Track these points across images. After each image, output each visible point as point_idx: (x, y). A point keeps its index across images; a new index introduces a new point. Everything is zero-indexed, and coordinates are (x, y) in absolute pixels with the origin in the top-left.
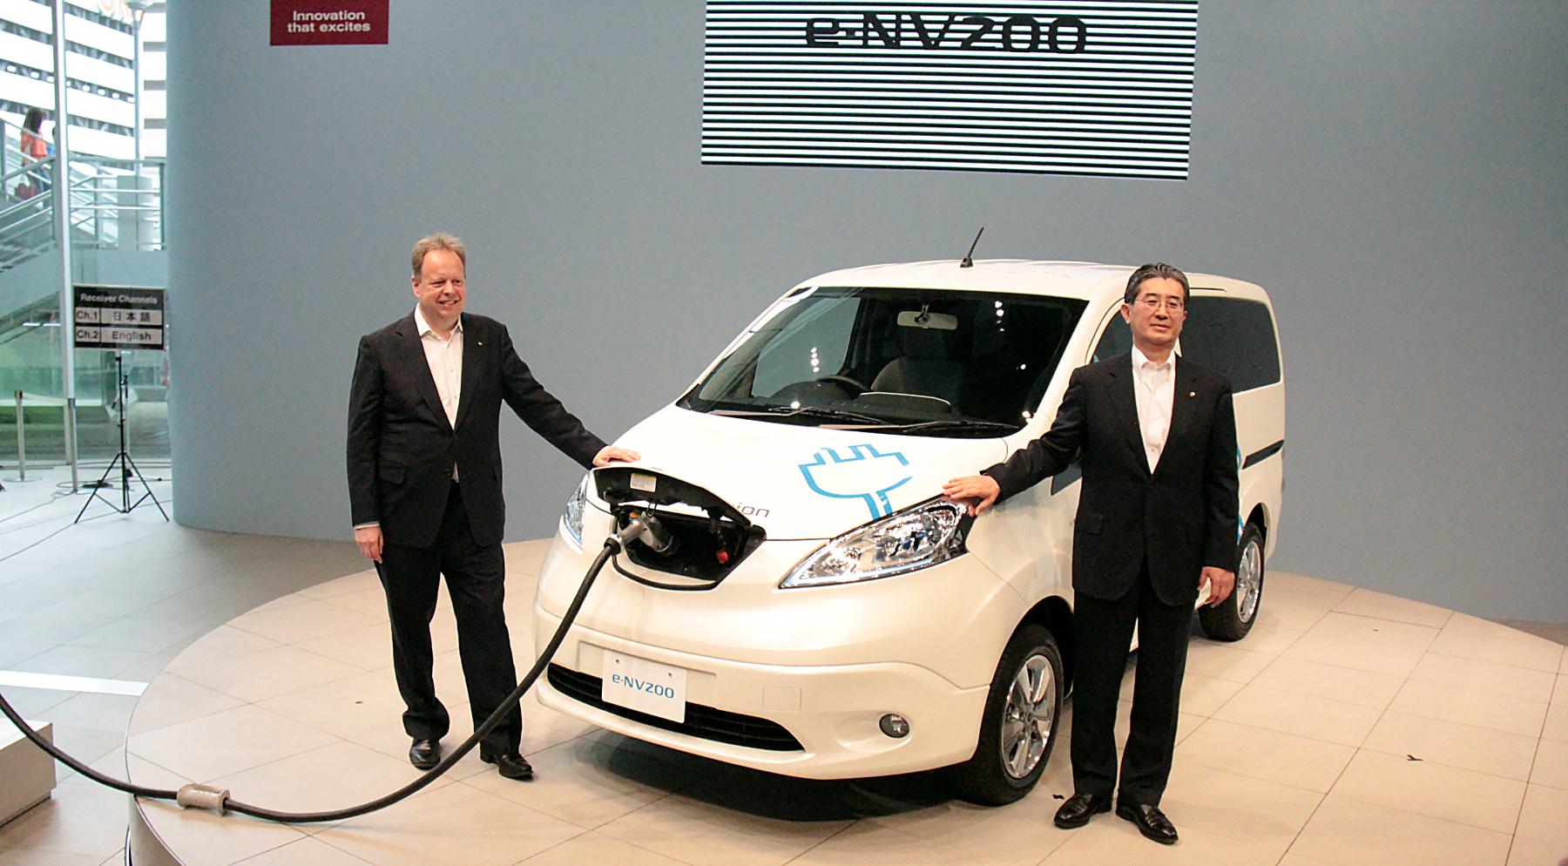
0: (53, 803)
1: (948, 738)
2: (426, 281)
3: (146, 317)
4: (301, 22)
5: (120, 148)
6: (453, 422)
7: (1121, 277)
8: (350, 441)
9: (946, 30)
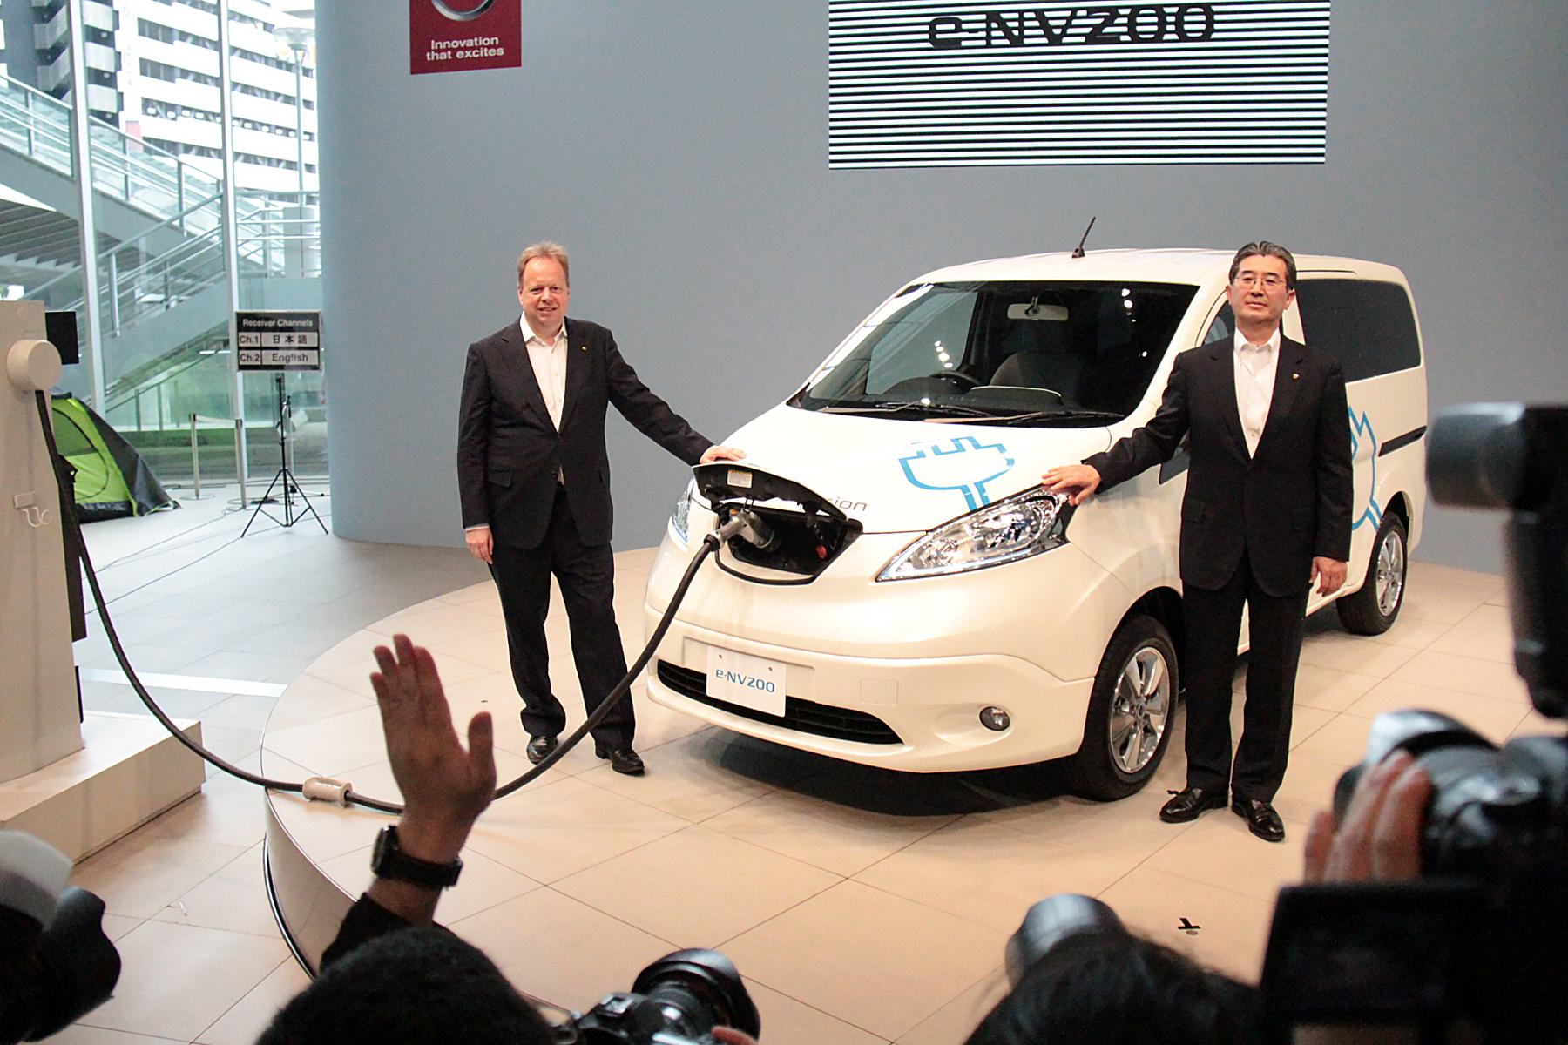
0: (204, 797)
1: (1055, 731)
2: (526, 289)
3: (303, 339)
4: (439, 51)
5: (285, 181)
6: (557, 426)
7: (1228, 258)
8: (462, 446)
9: (1069, 25)
